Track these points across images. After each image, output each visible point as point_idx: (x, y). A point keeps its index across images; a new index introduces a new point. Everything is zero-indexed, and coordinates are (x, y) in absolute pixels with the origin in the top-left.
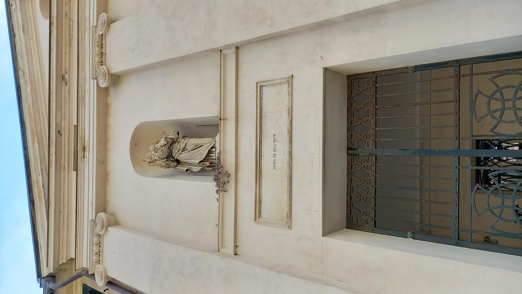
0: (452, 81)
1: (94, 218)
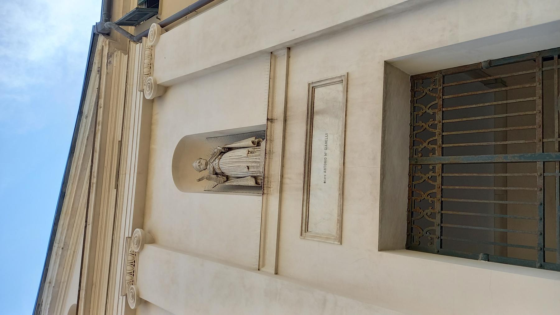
1: (130, 236)
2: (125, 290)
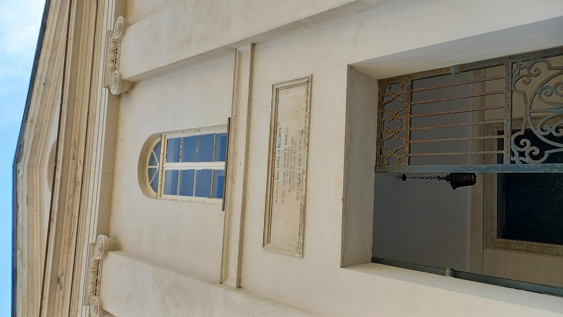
1: (94, 242)
2: (108, 82)
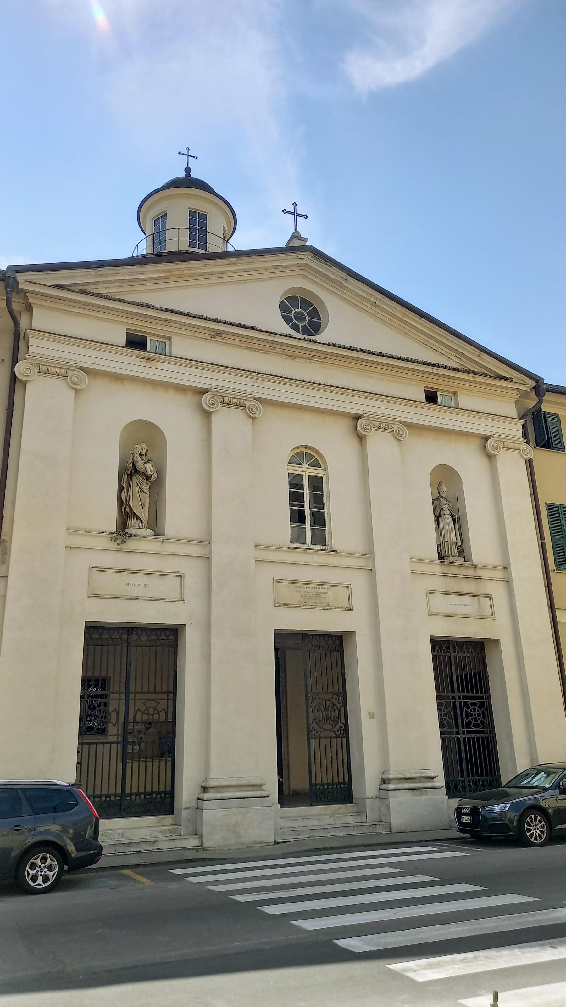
0: (166, 690)
